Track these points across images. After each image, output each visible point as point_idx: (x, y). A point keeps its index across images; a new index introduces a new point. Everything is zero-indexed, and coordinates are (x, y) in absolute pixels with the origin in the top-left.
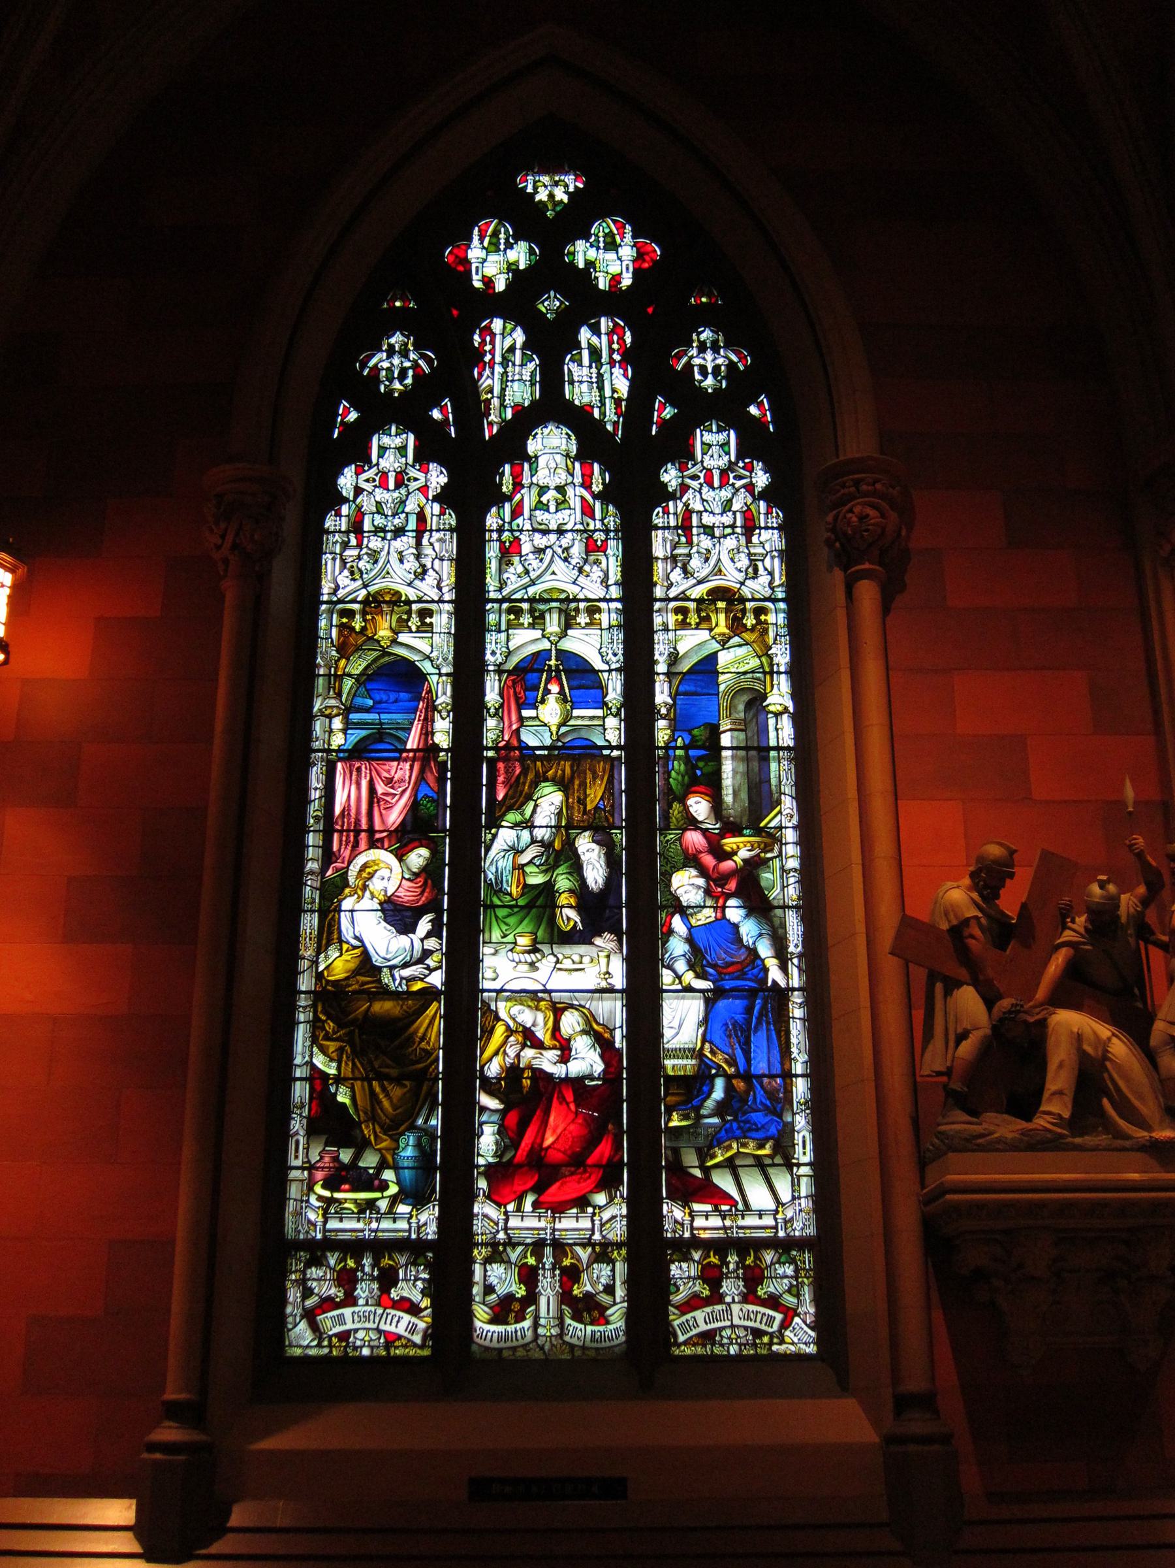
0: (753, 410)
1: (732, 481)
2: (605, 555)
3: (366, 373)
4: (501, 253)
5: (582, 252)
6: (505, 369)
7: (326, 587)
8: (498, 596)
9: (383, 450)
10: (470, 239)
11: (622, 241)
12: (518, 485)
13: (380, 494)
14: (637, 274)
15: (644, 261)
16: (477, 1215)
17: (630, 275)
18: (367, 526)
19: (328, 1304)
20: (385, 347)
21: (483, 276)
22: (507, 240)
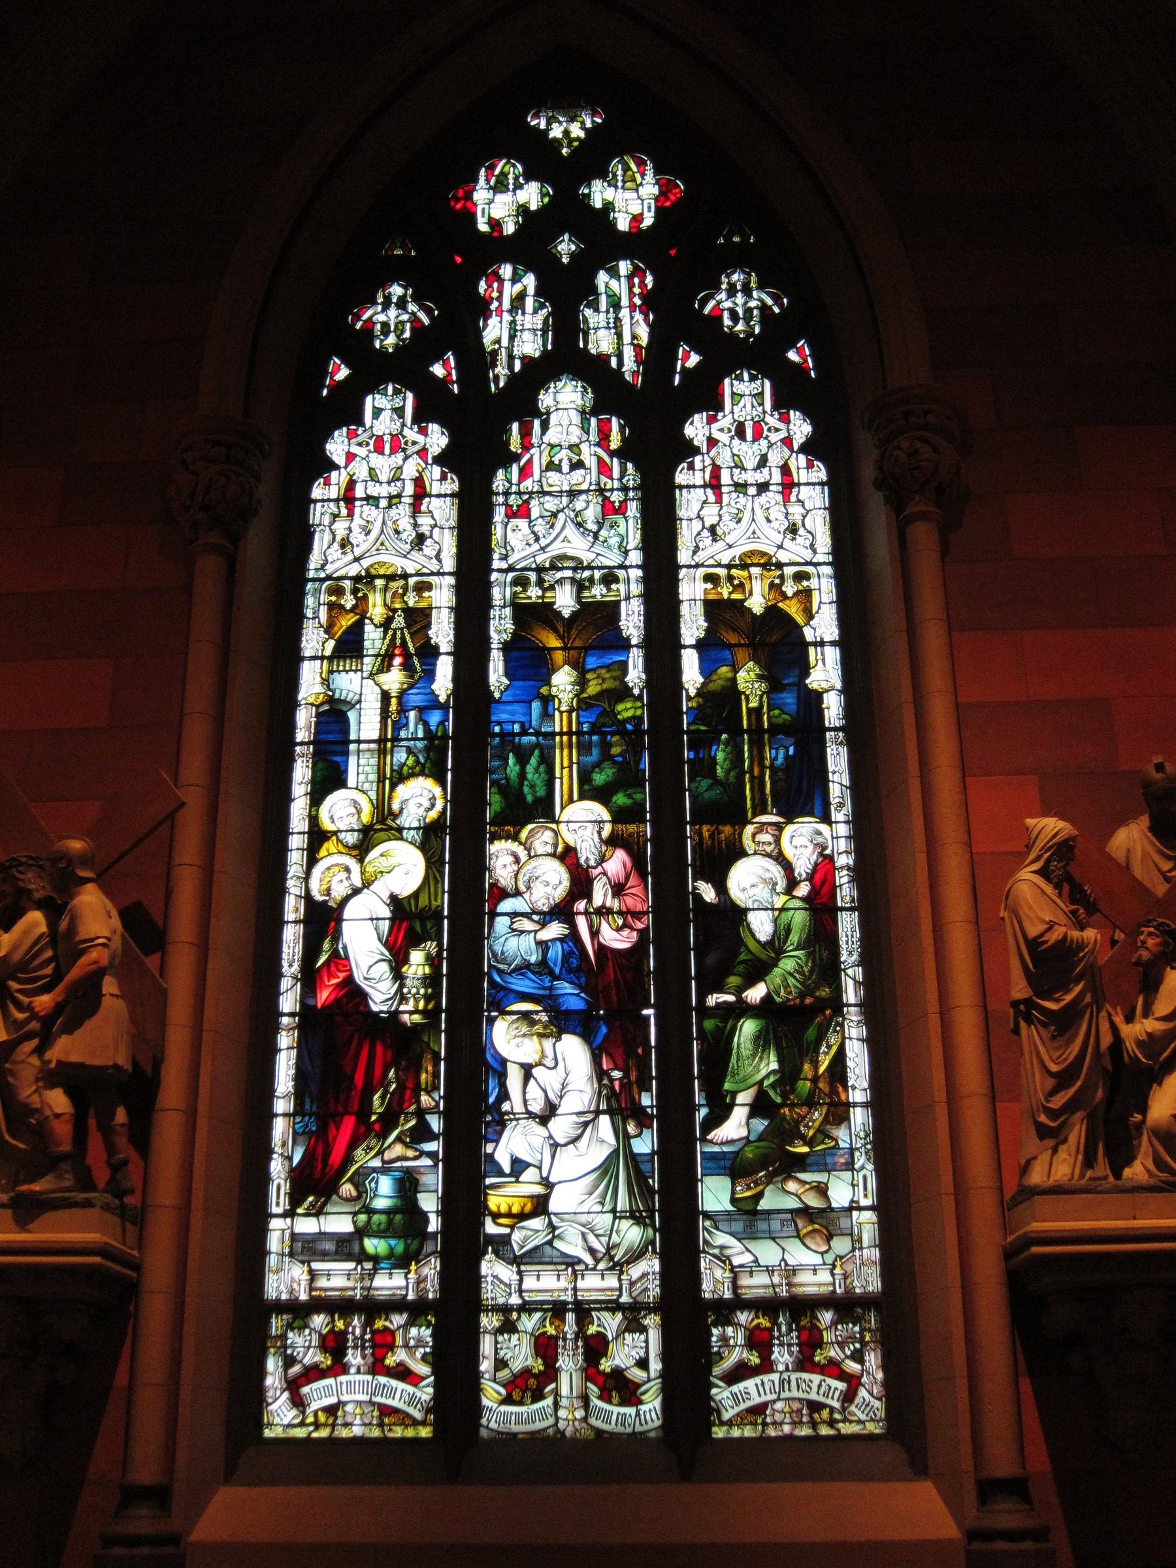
0: (792, 356)
1: (765, 433)
2: (626, 518)
3: (358, 326)
4: (510, 194)
5: (599, 193)
6: (514, 317)
7: (314, 560)
8: (504, 565)
9: (377, 412)
10: (476, 181)
11: (643, 179)
12: (527, 446)
13: (376, 460)
14: (660, 212)
15: (668, 199)
16: (486, 1277)
17: (652, 214)
18: (359, 492)
19: (314, 1373)
20: (380, 300)
21: (490, 218)
22: (516, 178)
